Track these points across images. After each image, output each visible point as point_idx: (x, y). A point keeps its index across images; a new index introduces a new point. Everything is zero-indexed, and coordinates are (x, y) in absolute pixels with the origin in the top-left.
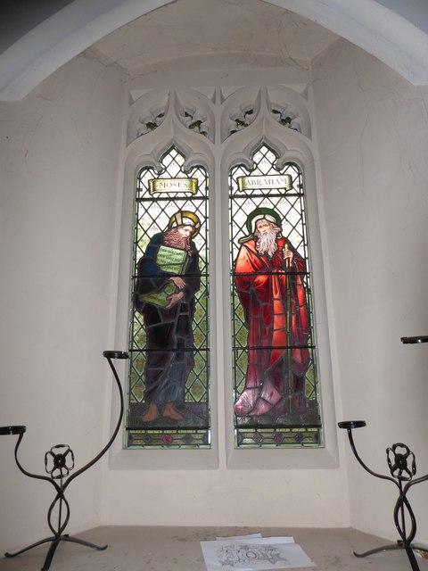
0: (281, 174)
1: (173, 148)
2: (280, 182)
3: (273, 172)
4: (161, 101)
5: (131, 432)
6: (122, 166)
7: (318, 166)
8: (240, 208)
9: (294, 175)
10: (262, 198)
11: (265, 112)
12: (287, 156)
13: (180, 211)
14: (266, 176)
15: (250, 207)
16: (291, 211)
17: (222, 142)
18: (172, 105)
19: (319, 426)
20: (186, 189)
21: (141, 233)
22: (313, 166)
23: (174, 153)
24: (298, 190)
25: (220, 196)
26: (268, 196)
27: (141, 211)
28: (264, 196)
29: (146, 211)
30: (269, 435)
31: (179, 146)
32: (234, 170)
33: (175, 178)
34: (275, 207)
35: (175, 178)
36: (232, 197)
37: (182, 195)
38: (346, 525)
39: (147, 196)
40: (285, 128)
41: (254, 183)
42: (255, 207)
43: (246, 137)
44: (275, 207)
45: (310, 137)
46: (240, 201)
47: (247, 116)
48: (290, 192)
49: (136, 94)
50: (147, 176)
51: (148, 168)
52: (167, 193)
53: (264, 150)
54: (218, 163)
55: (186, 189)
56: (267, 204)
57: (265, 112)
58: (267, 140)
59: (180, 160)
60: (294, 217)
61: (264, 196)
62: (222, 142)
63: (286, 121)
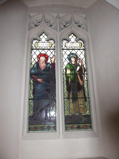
0: (48, 42)
1: (44, 33)
2: (77, 45)
3: (46, 42)
4: (39, 17)
5: (66, 125)
6: (27, 37)
7: (90, 41)
8: (65, 53)
9: (53, 43)
10: (67, 50)
11: (73, 23)
12: (50, 36)
13: (71, 53)
14: (73, 43)
15: (38, 53)
16: (81, 54)
17: (60, 31)
18: (43, 18)
19: (91, 123)
20: (78, 46)
21: (33, 60)
22: (88, 40)
23: (44, 34)
24: (54, 48)
25: (58, 49)
26: (74, 49)
27: (33, 53)
28: (73, 49)
29: (52, 53)
30: (52, 127)
31: (46, 33)
32: (63, 41)
33: (44, 42)
34: (76, 53)
35: (44, 42)
36: (63, 49)
37: (77, 48)
38: (100, 157)
39: (35, 48)
40: (50, 28)
41: (40, 45)
42: (70, 53)
43: (67, 31)
44: (76, 53)
45: (87, 31)
46: (65, 51)
47: (67, 24)
48: (81, 48)
49: (32, 14)
50: (34, 42)
51: (35, 39)
52: (42, 47)
53: (72, 35)
54: (58, 38)
55: (78, 46)
56: (43, 52)
57: (73, 23)
58: (73, 31)
59: (46, 37)
60: (82, 57)
61: (73, 49)
62: (60, 31)
63: (79, 26)
